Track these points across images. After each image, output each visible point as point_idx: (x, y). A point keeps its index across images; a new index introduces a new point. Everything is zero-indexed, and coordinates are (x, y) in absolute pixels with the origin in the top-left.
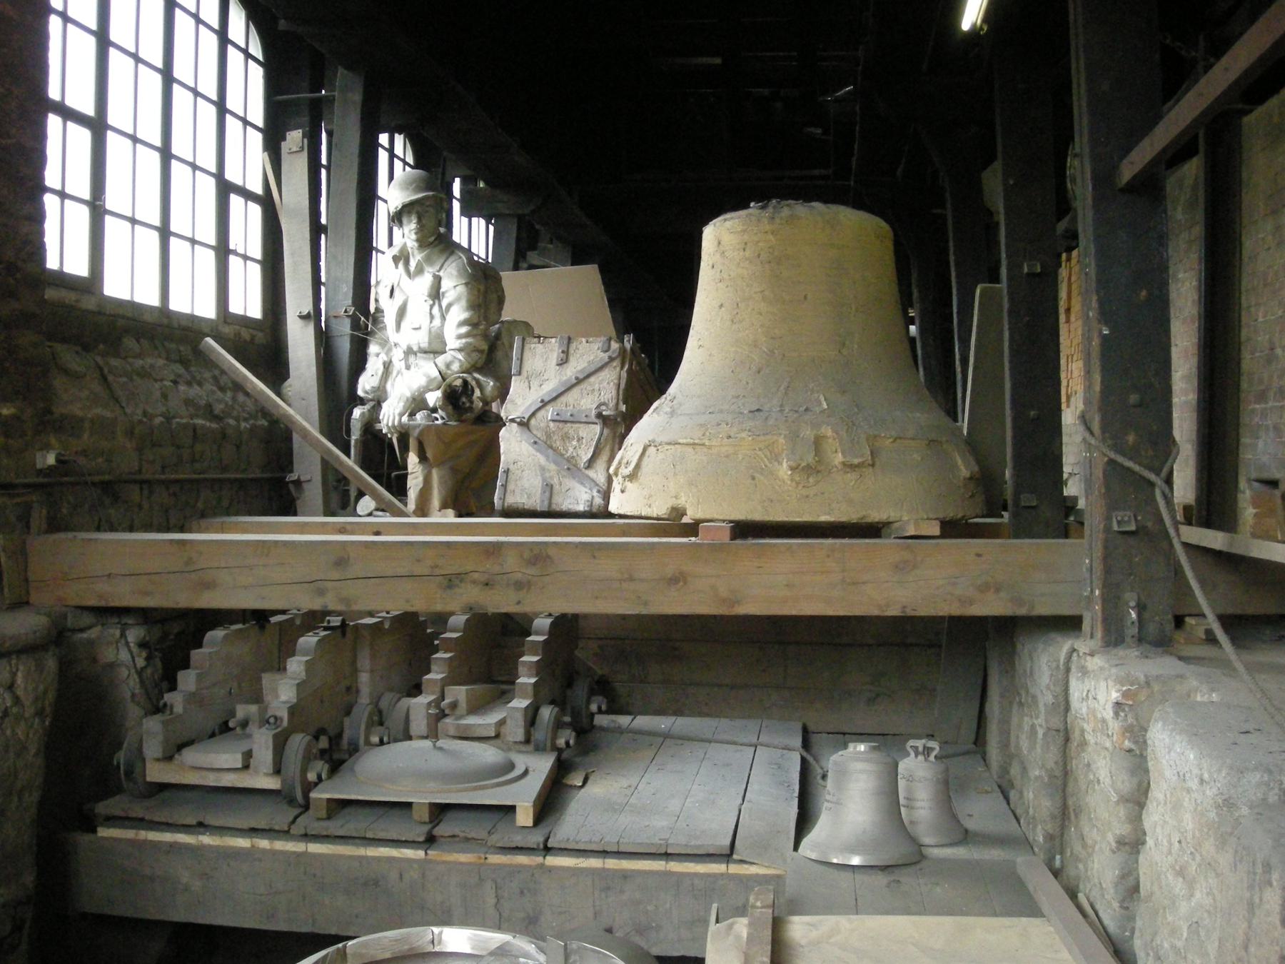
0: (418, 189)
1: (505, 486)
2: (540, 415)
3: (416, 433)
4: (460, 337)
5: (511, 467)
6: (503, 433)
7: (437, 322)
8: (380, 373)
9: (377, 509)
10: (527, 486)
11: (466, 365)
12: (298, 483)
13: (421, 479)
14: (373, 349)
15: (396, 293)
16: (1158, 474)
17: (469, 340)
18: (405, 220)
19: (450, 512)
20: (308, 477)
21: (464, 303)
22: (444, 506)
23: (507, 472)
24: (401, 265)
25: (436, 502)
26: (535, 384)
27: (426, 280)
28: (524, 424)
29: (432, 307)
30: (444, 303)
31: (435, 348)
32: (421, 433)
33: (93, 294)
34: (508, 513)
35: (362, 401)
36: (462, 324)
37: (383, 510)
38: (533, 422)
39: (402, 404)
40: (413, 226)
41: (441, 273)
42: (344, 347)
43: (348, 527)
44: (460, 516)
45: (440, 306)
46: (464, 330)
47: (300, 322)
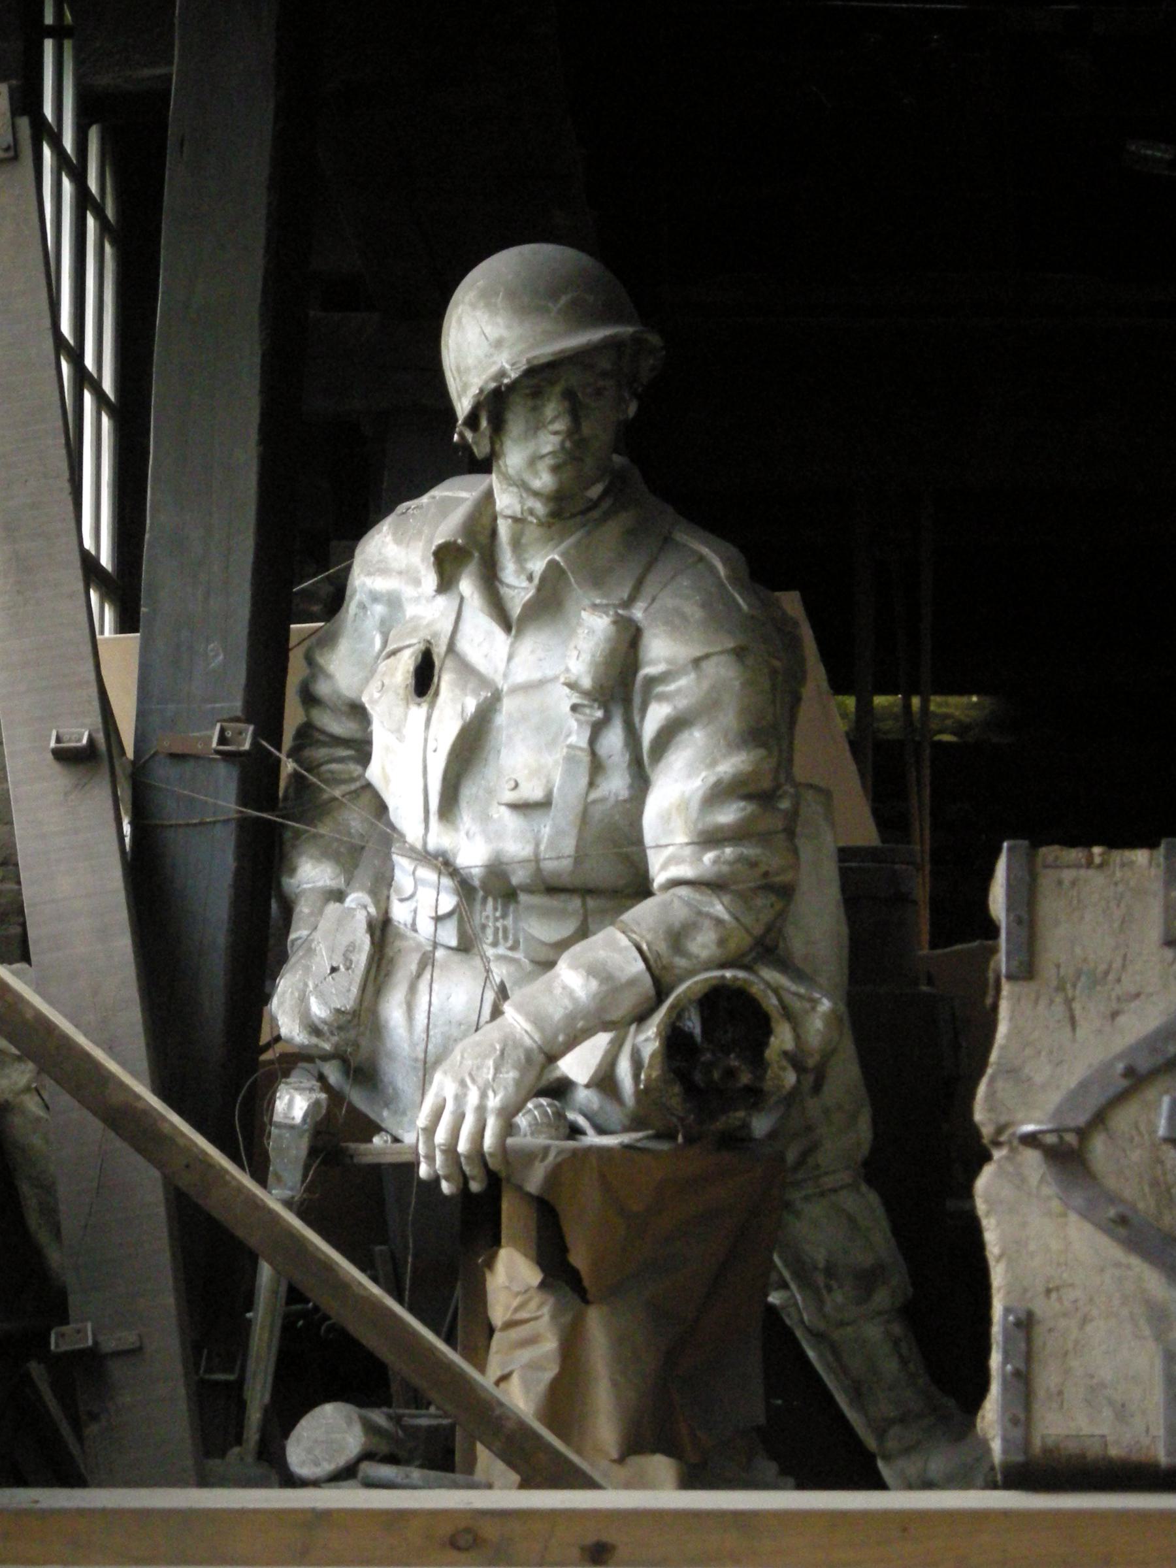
0: (581, 314)
1: (1022, 1382)
2: (1123, 1119)
3: (534, 1181)
4: (709, 839)
5: (1040, 1307)
6: (984, 1181)
7: (616, 784)
8: (361, 958)
9: (367, 1456)
10: (1106, 1373)
11: (740, 941)
12: (90, 1364)
13: (550, 1345)
14: (311, 874)
15: (446, 680)
16: (205, 1372)
17: (750, 851)
18: (515, 425)
19: (661, 1465)
20: (129, 1339)
21: (729, 718)
22: (639, 1441)
23: (1025, 1324)
24: (467, 586)
25: (606, 1430)
26: (1090, 1012)
27: (590, 630)
28: (1066, 1156)
29: (597, 730)
30: (655, 717)
31: (607, 877)
32: (554, 1177)
33: (661, 549)
34: (1027, 1474)
35: (293, 1061)
36: (718, 794)
37: (391, 1459)
38: (1099, 1146)
39: (510, 1075)
40: (548, 442)
41: (638, 613)
42: (209, 873)
43: (490, 1531)
44: (526, 1484)
45: (632, 735)
46: (728, 815)
47: (59, 778)
